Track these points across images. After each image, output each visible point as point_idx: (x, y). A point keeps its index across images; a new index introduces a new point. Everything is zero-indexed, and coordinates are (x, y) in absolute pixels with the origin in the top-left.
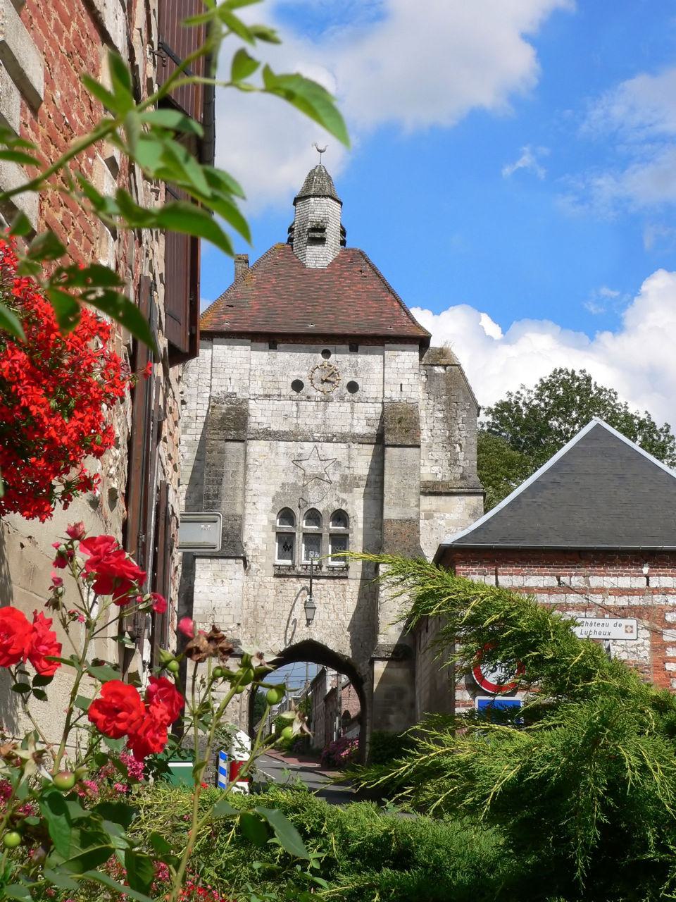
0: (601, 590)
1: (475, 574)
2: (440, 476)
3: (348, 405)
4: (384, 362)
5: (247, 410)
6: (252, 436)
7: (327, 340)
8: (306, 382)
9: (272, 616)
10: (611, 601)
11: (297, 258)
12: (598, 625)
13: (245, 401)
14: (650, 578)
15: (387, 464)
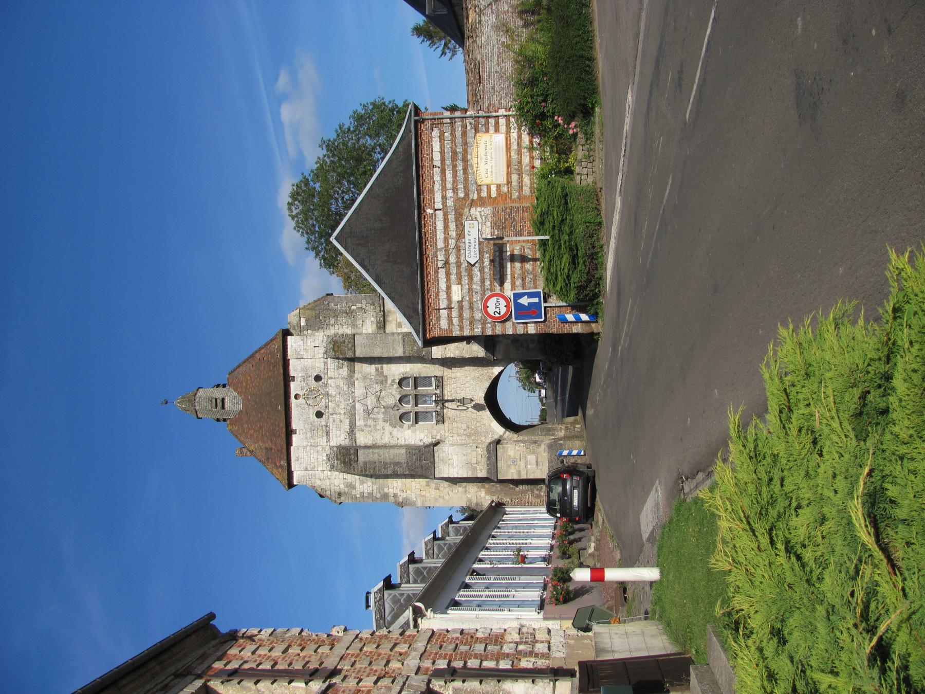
0: (446, 240)
1: (440, 324)
2: (373, 319)
3: (330, 381)
5: (337, 447)
8: (317, 409)
9: (469, 424)
10: (453, 233)
12: (470, 243)
13: (331, 448)
14: (436, 208)
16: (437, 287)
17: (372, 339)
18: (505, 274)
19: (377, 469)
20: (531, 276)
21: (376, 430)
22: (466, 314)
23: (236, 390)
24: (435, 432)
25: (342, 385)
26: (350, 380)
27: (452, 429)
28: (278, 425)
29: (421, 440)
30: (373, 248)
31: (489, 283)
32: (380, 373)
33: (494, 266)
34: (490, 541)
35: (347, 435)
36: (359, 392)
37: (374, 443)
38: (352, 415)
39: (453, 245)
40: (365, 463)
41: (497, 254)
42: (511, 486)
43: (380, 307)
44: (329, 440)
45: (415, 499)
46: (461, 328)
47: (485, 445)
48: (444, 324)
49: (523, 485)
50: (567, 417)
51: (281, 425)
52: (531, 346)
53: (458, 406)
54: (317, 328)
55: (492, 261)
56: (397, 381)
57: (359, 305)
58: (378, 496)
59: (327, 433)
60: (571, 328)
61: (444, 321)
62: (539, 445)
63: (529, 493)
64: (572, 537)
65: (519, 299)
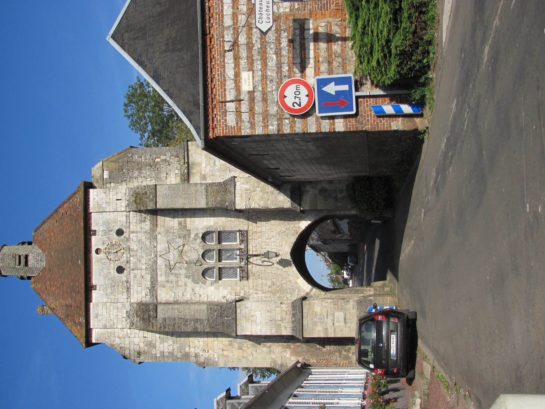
0: (235, 16)
1: (226, 120)
2: (177, 171)
4: (103, 212)
5: (137, 304)
6: (155, 299)
7: (89, 251)
8: (118, 264)
9: (274, 280)
11: (39, 273)
12: (261, 8)
13: (131, 304)
15: (169, 207)
16: (223, 75)
17: (174, 190)
18: (307, 57)
19: (176, 326)
20: (340, 60)
21: (178, 286)
22: (259, 108)
23: (40, 247)
24: (238, 289)
25: (144, 239)
26: (153, 236)
27: (257, 286)
28: (79, 280)
29: (224, 297)
30: (151, 38)
31: (287, 68)
32: (183, 227)
33: (294, 48)
34: (291, 400)
35: (148, 291)
36: (161, 247)
37: (176, 300)
38: (153, 270)
39: (243, 23)
40: (165, 320)
41: (298, 32)
42: (318, 346)
43: (184, 159)
44: (130, 297)
45: (217, 360)
46: (253, 125)
47: (290, 302)
48: (231, 119)
49: (330, 345)
50: (374, 282)
51: (81, 280)
52: (340, 196)
53: (263, 262)
54: (120, 181)
55: (291, 41)
56: (201, 235)
57: (163, 157)
58: (179, 355)
59: (128, 288)
60: (390, 124)
61: (232, 116)
62: (348, 301)
63: (337, 354)
64: (387, 397)
65: (323, 87)
